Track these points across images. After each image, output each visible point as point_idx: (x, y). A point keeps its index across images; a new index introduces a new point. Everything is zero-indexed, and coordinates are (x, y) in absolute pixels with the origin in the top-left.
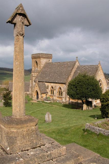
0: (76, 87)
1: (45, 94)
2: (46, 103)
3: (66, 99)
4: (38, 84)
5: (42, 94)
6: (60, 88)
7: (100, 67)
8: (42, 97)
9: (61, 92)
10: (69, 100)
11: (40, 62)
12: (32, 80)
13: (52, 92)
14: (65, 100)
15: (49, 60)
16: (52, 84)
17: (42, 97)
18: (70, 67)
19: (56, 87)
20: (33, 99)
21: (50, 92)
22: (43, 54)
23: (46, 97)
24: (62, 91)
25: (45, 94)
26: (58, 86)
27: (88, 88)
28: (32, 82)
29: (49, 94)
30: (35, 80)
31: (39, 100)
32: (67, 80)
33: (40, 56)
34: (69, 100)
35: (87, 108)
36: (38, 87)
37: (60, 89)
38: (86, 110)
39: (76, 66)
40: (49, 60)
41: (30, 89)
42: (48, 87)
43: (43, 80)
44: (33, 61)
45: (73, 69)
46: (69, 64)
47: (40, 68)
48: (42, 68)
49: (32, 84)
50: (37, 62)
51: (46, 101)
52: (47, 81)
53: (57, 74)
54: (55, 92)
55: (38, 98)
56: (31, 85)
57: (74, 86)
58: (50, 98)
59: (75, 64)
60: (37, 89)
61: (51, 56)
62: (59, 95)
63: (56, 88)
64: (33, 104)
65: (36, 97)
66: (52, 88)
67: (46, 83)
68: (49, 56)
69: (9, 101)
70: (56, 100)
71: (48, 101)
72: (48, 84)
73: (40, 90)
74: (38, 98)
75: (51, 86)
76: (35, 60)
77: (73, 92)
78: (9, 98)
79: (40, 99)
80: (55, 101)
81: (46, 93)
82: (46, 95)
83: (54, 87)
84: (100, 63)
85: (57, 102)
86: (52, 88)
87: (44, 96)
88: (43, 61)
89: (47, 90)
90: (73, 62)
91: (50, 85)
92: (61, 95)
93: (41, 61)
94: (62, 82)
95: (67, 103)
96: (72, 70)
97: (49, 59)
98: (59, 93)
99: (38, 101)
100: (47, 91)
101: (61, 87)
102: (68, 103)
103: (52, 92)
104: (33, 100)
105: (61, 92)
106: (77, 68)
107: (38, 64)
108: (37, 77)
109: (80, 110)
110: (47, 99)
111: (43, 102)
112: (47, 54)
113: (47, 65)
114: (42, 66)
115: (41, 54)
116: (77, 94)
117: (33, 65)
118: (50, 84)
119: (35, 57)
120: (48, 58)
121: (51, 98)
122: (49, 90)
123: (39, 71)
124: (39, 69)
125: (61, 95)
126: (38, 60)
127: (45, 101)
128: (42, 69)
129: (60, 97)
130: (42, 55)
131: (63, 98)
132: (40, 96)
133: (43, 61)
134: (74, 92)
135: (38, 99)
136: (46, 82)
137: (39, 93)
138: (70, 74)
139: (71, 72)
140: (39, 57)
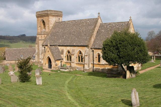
0: (117, 49)
1: (60, 61)
2: (64, 72)
3: (104, 65)
4: (50, 49)
5: (56, 60)
6: (80, 52)
7: (131, 23)
8: (56, 65)
9: (82, 57)
10: (93, 67)
11: (49, 21)
12: (38, 44)
13: (69, 58)
14: (89, 67)
15: (59, 19)
16: (69, 48)
17: (56, 65)
18: (90, 25)
19: (73, 51)
20: (43, 68)
21: (66, 59)
22: (52, 11)
23: (61, 65)
24: (83, 56)
25: (60, 61)
26: (77, 49)
27: (134, 49)
28: (38, 46)
29: (65, 60)
30: (43, 43)
31: (52, 69)
32: (89, 41)
33: (49, 14)
34: (93, 67)
35: (130, 76)
36: (50, 52)
37: (80, 52)
38: (131, 79)
39: (98, 25)
40: (59, 19)
41: (36, 56)
42: (63, 51)
43: (55, 44)
44: (38, 20)
45: (95, 27)
46: (88, 21)
47: (49, 29)
48: (51, 28)
49: (38, 49)
50: (43, 22)
51: (63, 70)
52: (60, 45)
53: (73, 34)
54: (73, 57)
55: (50, 66)
56: (37, 51)
57: (114, 47)
58: (67, 65)
59: (97, 21)
60: (49, 54)
61: (61, 13)
62: (79, 61)
63: (74, 52)
64: (50, 74)
65: (47, 65)
66: (69, 52)
67: (59, 47)
68: (58, 14)
69: (28, 73)
70: (75, 68)
71: (66, 69)
72: (62, 48)
73: (53, 56)
74: (50, 66)
75: (66, 51)
76: (42, 18)
77: (113, 56)
78: (28, 69)
79: (54, 67)
80: (74, 69)
81: (61, 59)
82: (61, 62)
83: (71, 51)
84: (131, 19)
85: (77, 69)
86: (69, 53)
87: (59, 63)
88: (52, 20)
89: (62, 55)
90: (94, 19)
91: (65, 49)
92: (82, 61)
93: (50, 19)
94: (82, 44)
95: (91, 71)
96: (94, 29)
97: (59, 18)
98: (94, 59)
99: (52, 71)
100: (61, 57)
101: (82, 51)
102: (91, 70)
103: (69, 58)
104: (44, 69)
105: (82, 57)
106: (100, 27)
107: (46, 24)
108: (45, 40)
109: (121, 79)
110: (62, 67)
111: (56, 71)
112: (57, 11)
113: (58, 24)
114: (51, 26)
115: (50, 11)
116: (120, 58)
117: (39, 25)
118: (64, 47)
119: (41, 15)
120: (57, 16)
121: (68, 65)
122: (64, 56)
123: (46, 32)
124: (47, 30)
125: (82, 61)
126: (45, 19)
127: (61, 70)
128: (51, 30)
129: (80, 63)
130: (51, 12)
131: (85, 65)
132: (53, 64)
133: (52, 20)
134: (116, 56)
135: (51, 68)
136: (59, 46)
137: (52, 60)
138: (93, 34)
139: (93, 32)
140: (47, 15)
